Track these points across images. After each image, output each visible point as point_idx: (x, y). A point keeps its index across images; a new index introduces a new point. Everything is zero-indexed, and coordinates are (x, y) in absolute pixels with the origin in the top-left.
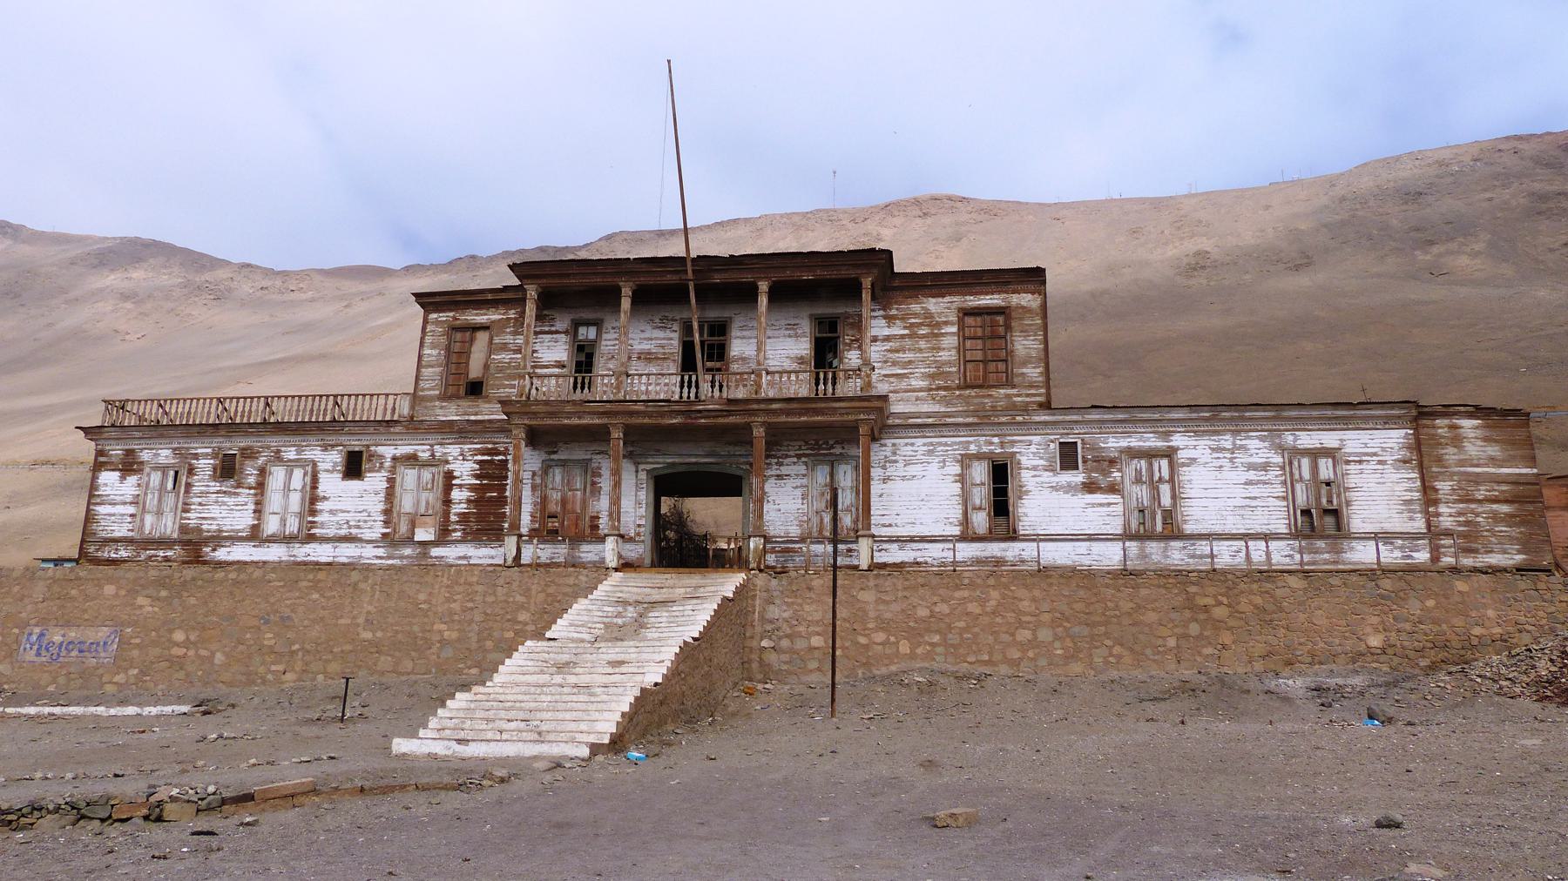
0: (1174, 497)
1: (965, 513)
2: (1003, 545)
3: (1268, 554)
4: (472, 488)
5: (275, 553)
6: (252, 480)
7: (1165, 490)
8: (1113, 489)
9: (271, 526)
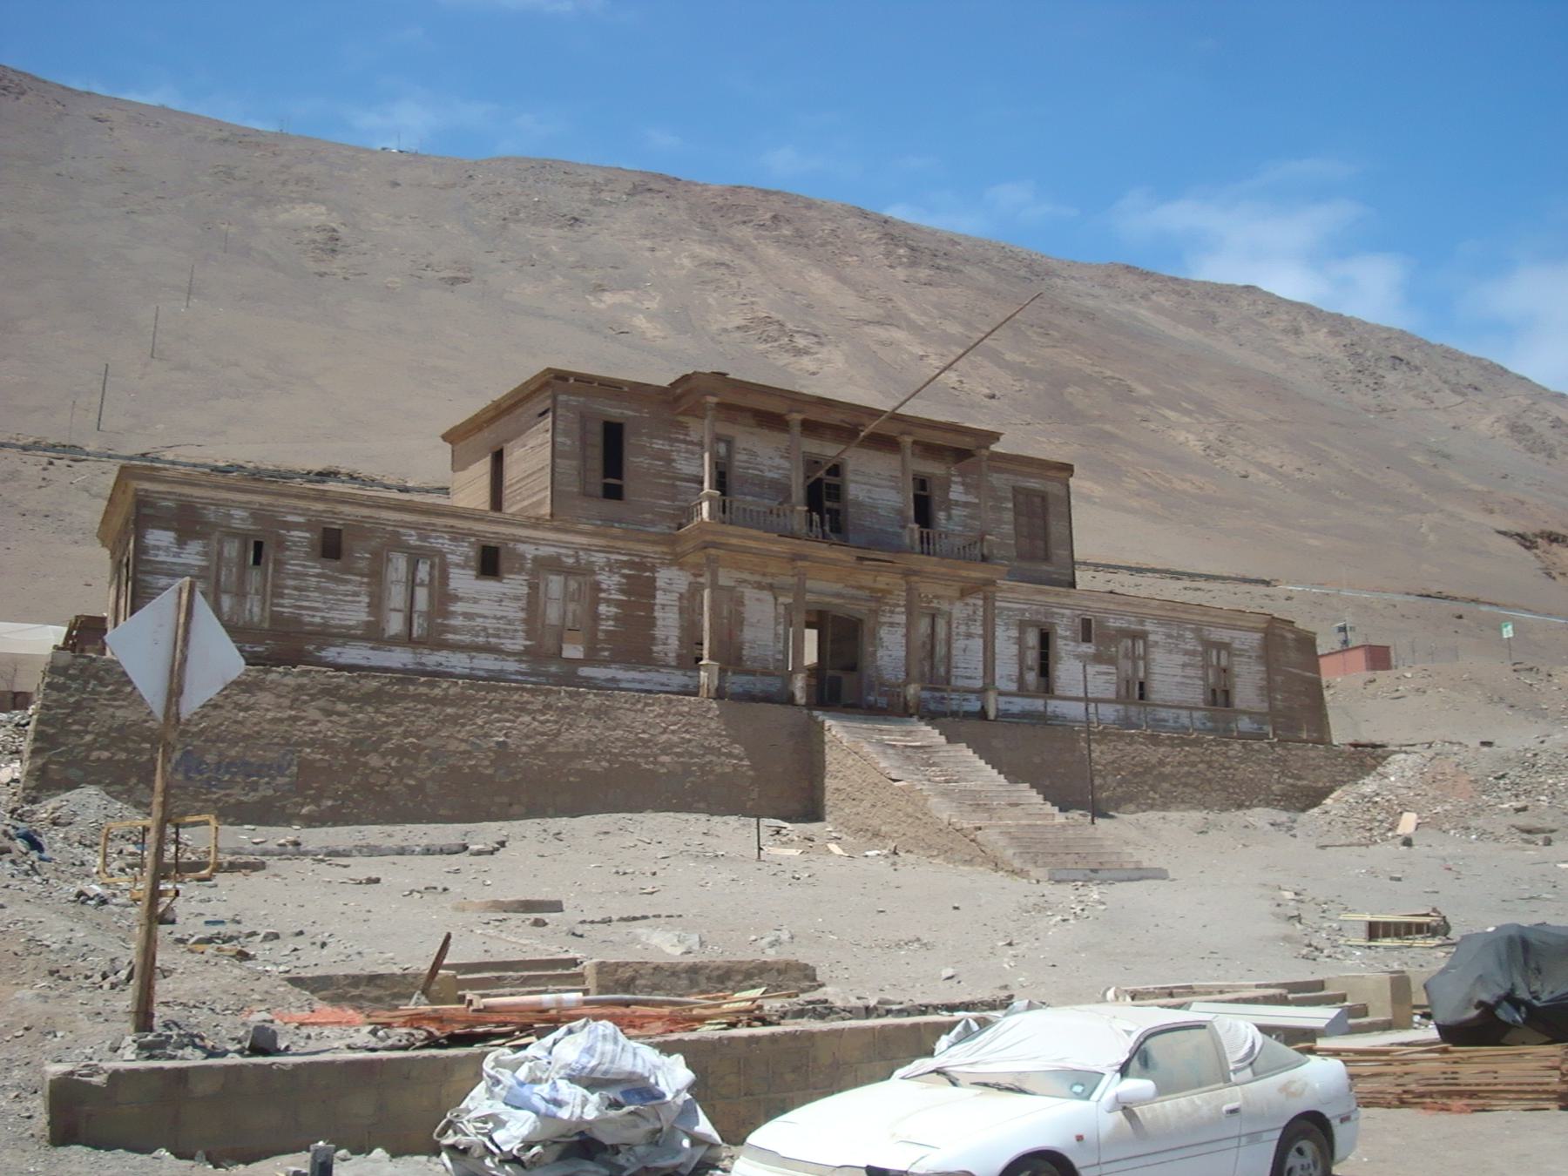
4: (618, 604)
5: (399, 658)
7: (1141, 663)
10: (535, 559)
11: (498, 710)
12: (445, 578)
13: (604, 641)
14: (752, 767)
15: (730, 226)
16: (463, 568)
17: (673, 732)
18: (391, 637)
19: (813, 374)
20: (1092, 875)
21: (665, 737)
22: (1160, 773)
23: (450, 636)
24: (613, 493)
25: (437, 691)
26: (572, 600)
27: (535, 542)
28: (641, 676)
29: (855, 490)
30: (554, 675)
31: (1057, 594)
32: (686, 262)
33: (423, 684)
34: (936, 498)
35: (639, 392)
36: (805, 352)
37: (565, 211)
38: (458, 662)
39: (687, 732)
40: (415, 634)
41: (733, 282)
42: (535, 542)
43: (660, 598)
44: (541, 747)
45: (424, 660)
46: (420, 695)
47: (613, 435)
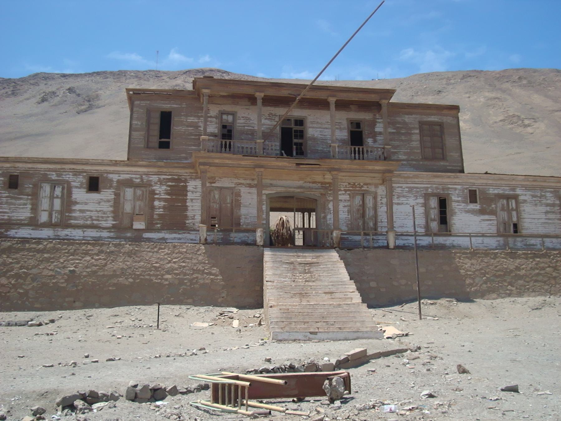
0: (518, 217)
1: (427, 222)
2: (445, 238)
3: (433, 240)
4: (165, 200)
5: (46, 233)
6: (28, 191)
7: (514, 213)
8: (493, 213)
9: (44, 217)
10: (118, 181)
11: (73, 254)
12: (70, 193)
13: (158, 219)
14: (223, 280)
15: (502, 84)
16: (80, 188)
17: (175, 263)
18: (41, 224)
19: (532, 133)
20: (312, 336)
21: (169, 265)
22: (516, 275)
23: (72, 221)
24: (164, 145)
25: (40, 246)
26: (139, 200)
27: (118, 173)
28: (180, 236)
29: (312, 131)
30: (129, 238)
31: (449, 177)
32: (482, 100)
33: (33, 243)
34: (366, 132)
35: (176, 95)
36: (529, 125)
37: (435, 89)
38: (77, 234)
39: (183, 262)
40: (53, 222)
41: (500, 104)
42: (118, 173)
43: (190, 196)
44: (94, 272)
45: (59, 233)
46: (31, 248)
47: (166, 119)
